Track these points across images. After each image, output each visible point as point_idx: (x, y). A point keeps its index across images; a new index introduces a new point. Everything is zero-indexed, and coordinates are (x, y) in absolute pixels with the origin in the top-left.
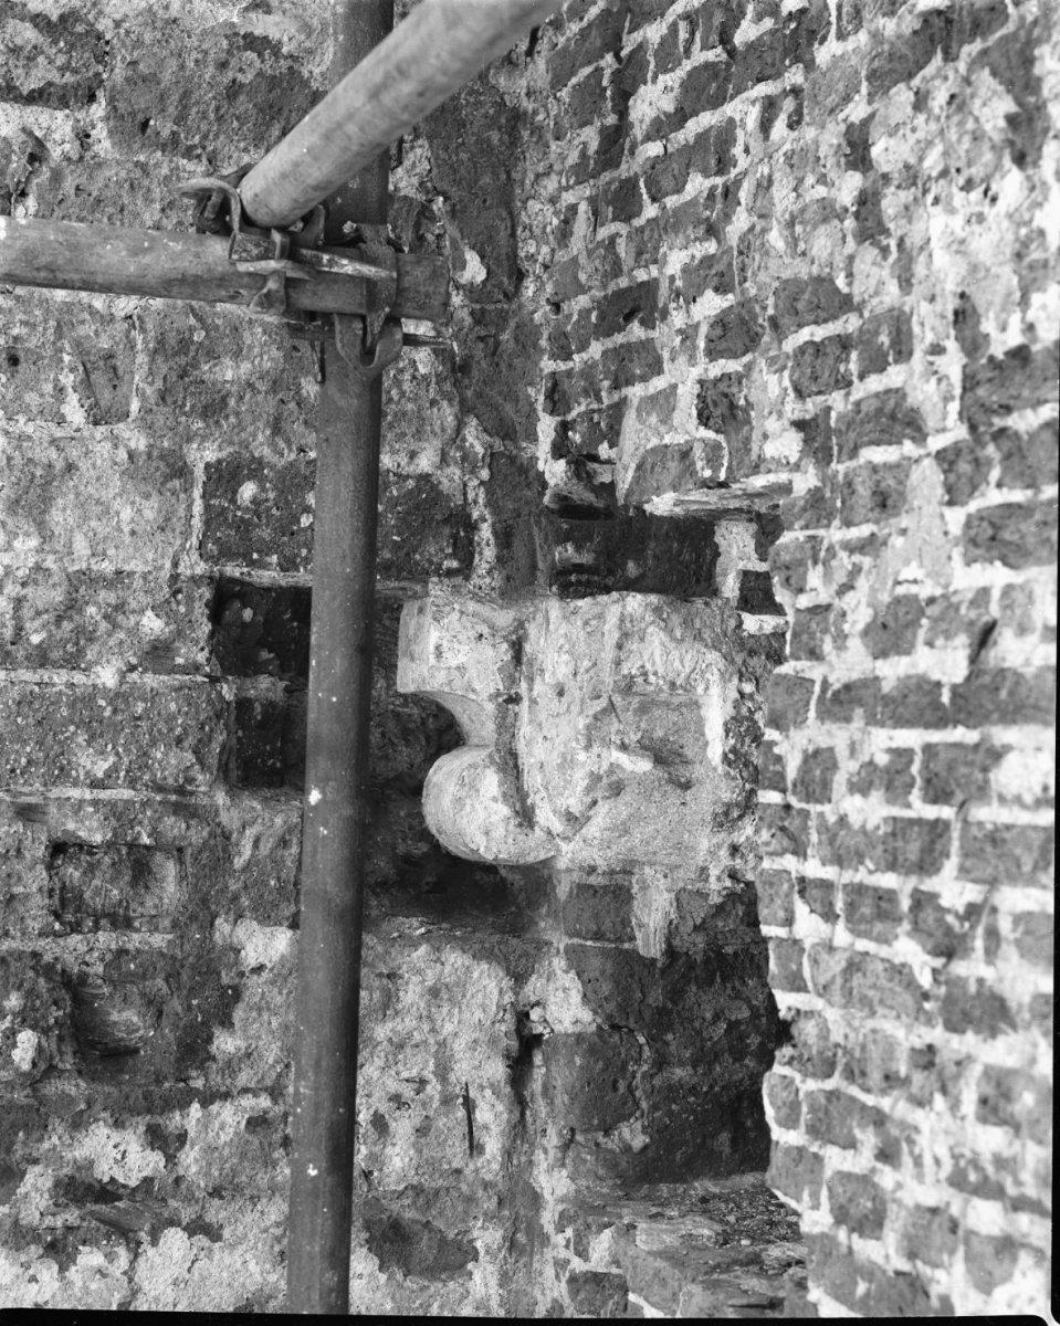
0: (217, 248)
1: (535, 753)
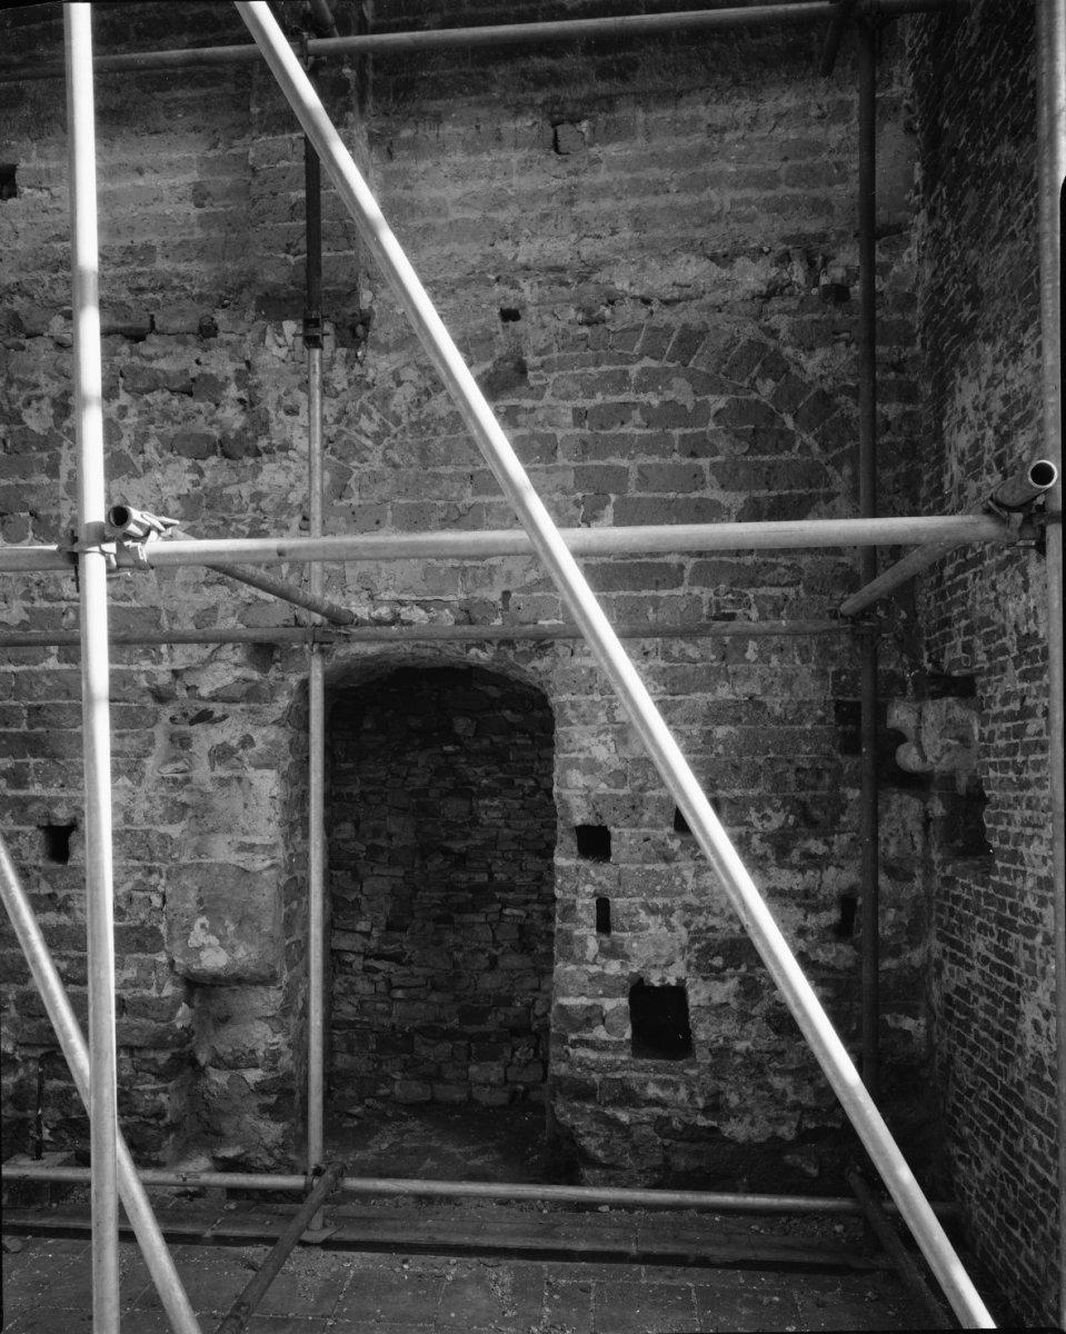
0: (835, 623)
1: (927, 741)
